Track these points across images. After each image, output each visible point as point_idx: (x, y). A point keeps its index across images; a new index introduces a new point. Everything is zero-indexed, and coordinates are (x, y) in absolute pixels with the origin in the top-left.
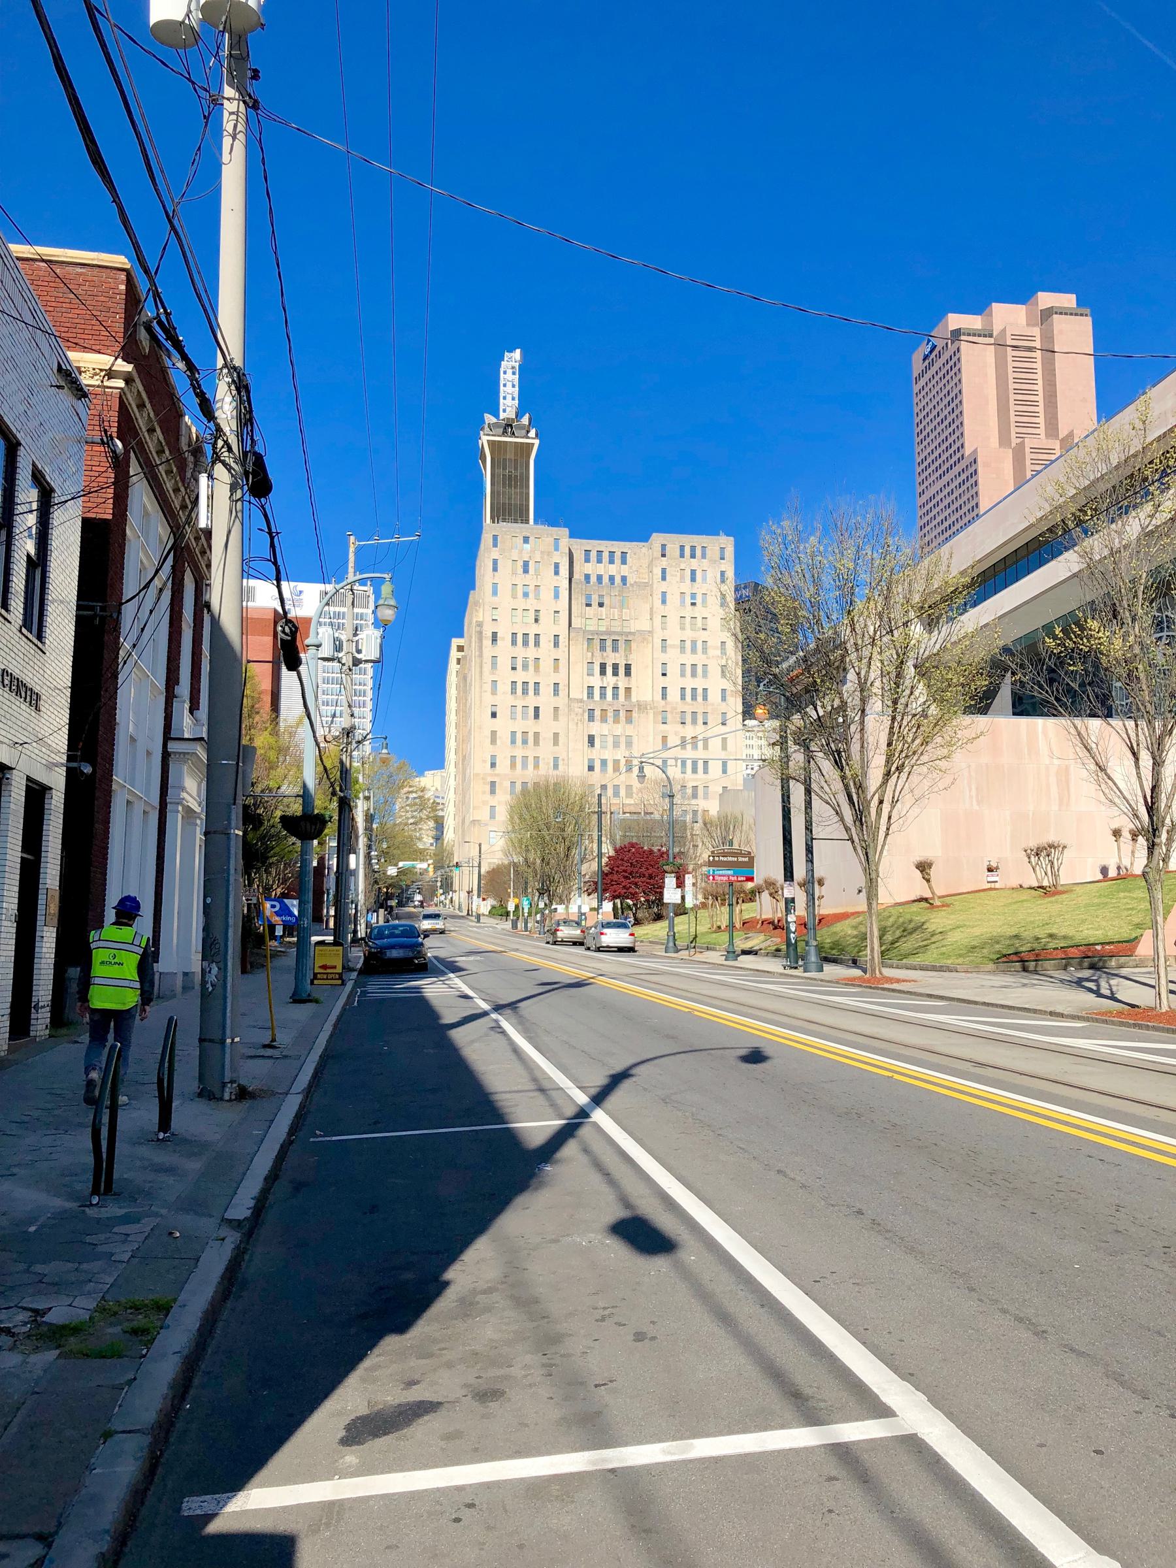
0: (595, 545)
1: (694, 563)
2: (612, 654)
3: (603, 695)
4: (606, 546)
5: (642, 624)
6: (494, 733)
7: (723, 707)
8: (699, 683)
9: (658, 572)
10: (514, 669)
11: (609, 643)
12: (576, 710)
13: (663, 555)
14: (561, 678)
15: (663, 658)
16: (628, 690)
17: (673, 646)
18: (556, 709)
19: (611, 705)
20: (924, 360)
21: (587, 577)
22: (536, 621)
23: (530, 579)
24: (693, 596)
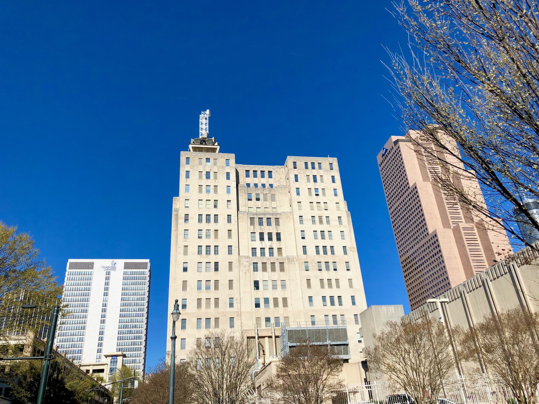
0: (252, 168)
1: (315, 172)
2: (267, 228)
4: (259, 168)
5: (286, 208)
6: (185, 282)
7: (346, 258)
9: (292, 178)
10: (200, 238)
11: (265, 220)
12: (245, 263)
14: (233, 242)
15: (302, 227)
16: (280, 249)
18: (230, 263)
19: (268, 259)
22: (215, 206)
24: (316, 189)
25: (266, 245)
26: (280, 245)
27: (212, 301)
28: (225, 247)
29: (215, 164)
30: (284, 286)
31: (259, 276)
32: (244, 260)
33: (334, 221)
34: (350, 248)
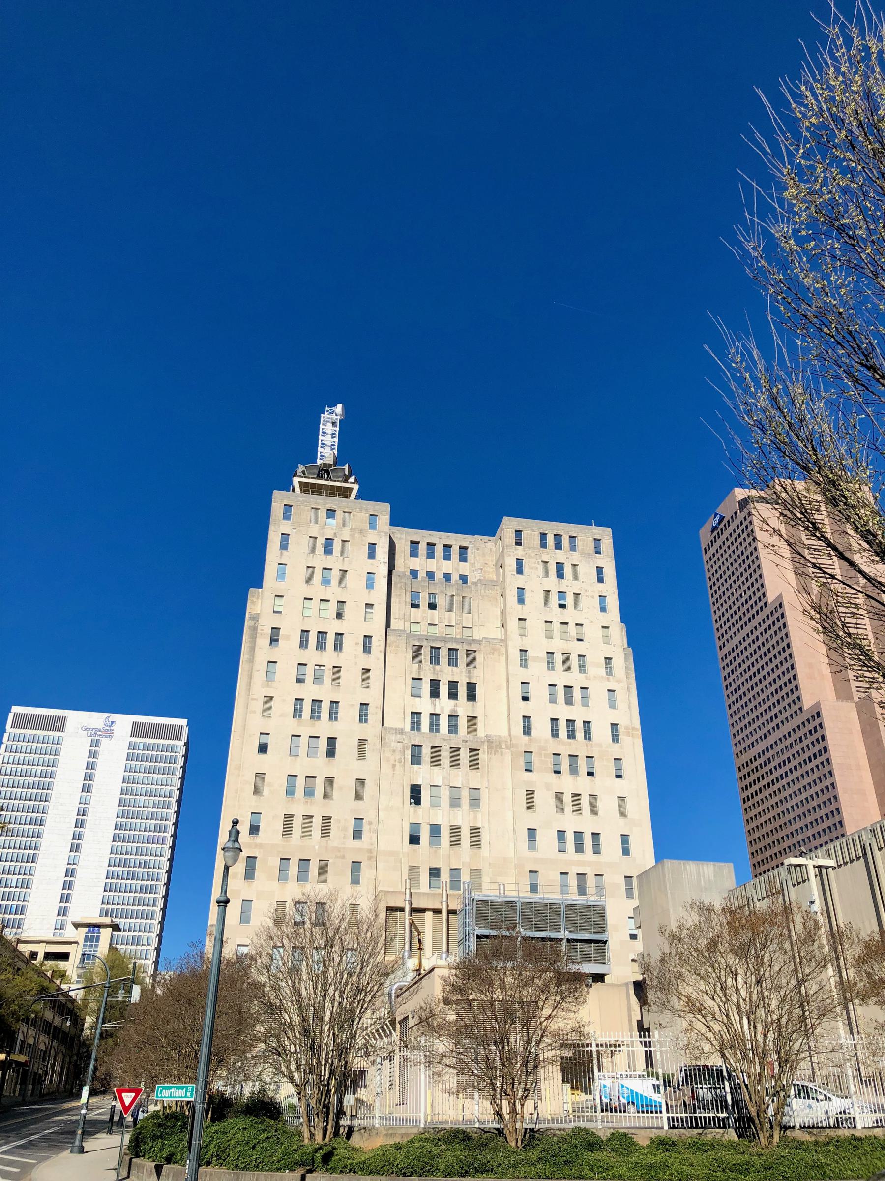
0: (424, 537)
1: (560, 556)
3: (434, 726)
4: (440, 538)
7: (616, 750)
8: (578, 713)
9: (511, 564)
10: (300, 680)
11: (444, 653)
13: (519, 543)
14: (372, 696)
16: (472, 719)
17: (536, 659)
18: (362, 742)
20: (712, 532)
21: (414, 574)
22: (339, 615)
23: (334, 562)
24: (562, 594)
25: (442, 709)
26: (473, 711)
27: (317, 823)
28: (353, 705)
29: (346, 523)
30: (475, 802)
31: (423, 775)
32: (393, 737)
33: (596, 669)
34: (627, 728)
